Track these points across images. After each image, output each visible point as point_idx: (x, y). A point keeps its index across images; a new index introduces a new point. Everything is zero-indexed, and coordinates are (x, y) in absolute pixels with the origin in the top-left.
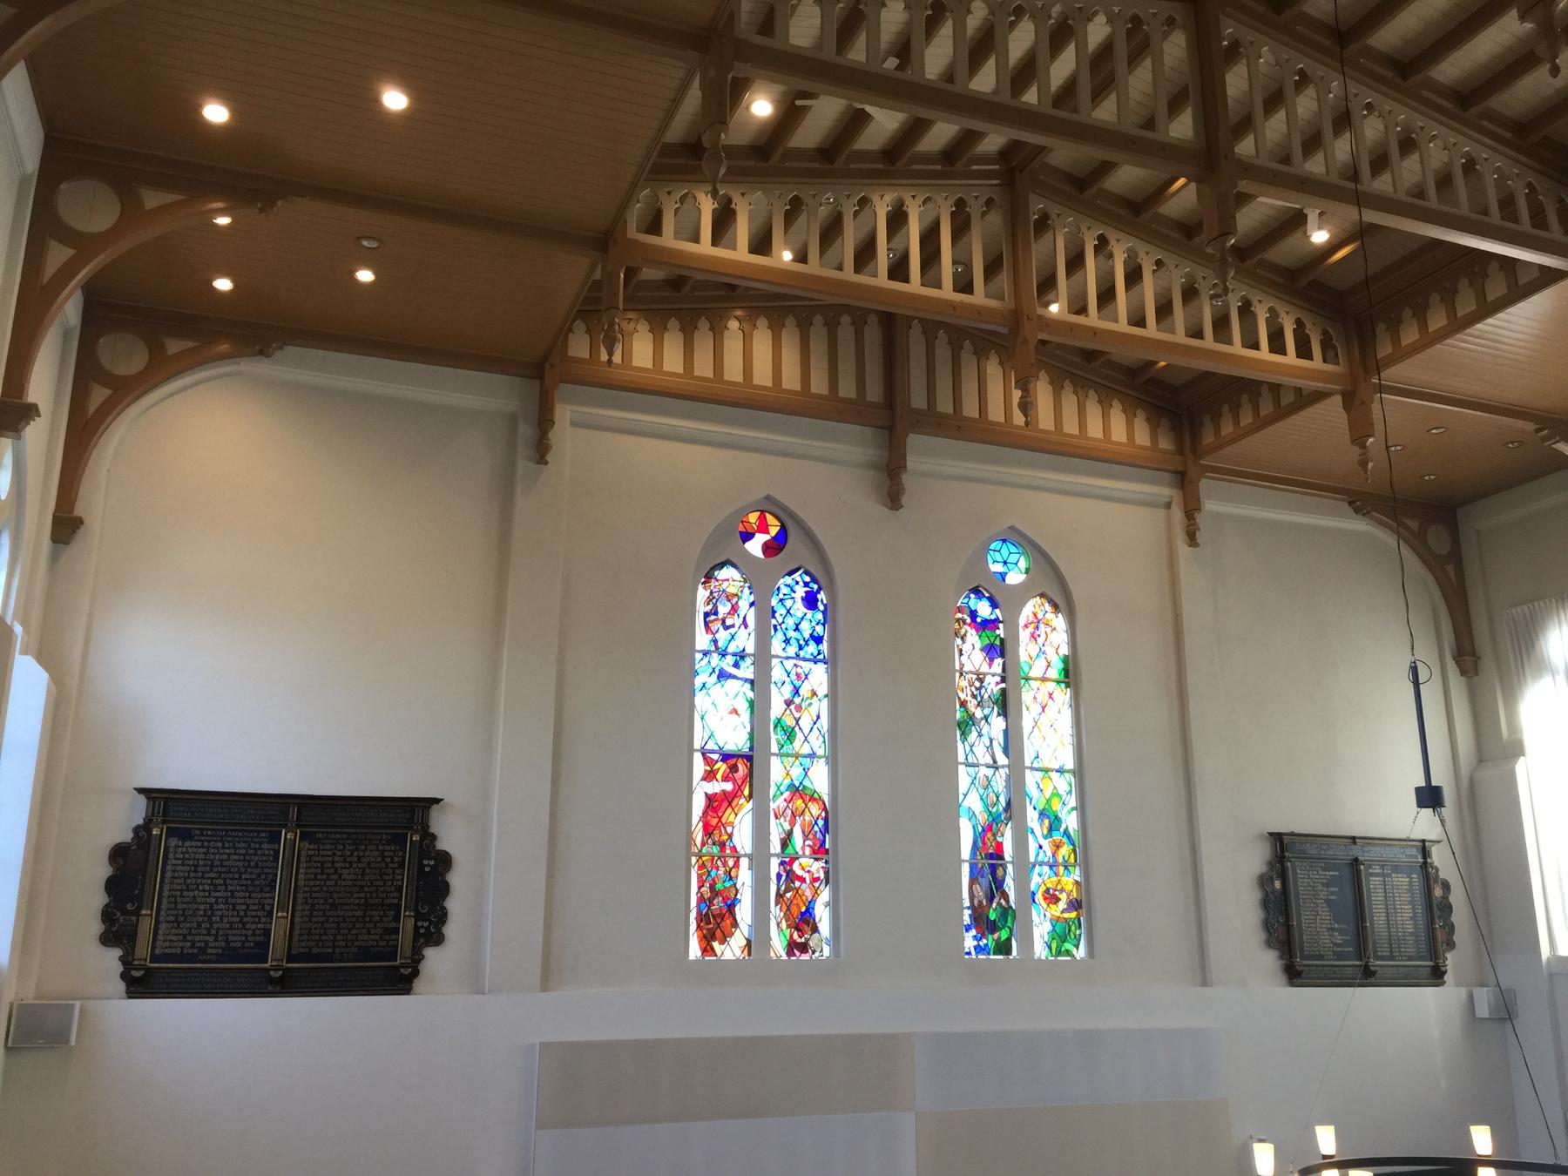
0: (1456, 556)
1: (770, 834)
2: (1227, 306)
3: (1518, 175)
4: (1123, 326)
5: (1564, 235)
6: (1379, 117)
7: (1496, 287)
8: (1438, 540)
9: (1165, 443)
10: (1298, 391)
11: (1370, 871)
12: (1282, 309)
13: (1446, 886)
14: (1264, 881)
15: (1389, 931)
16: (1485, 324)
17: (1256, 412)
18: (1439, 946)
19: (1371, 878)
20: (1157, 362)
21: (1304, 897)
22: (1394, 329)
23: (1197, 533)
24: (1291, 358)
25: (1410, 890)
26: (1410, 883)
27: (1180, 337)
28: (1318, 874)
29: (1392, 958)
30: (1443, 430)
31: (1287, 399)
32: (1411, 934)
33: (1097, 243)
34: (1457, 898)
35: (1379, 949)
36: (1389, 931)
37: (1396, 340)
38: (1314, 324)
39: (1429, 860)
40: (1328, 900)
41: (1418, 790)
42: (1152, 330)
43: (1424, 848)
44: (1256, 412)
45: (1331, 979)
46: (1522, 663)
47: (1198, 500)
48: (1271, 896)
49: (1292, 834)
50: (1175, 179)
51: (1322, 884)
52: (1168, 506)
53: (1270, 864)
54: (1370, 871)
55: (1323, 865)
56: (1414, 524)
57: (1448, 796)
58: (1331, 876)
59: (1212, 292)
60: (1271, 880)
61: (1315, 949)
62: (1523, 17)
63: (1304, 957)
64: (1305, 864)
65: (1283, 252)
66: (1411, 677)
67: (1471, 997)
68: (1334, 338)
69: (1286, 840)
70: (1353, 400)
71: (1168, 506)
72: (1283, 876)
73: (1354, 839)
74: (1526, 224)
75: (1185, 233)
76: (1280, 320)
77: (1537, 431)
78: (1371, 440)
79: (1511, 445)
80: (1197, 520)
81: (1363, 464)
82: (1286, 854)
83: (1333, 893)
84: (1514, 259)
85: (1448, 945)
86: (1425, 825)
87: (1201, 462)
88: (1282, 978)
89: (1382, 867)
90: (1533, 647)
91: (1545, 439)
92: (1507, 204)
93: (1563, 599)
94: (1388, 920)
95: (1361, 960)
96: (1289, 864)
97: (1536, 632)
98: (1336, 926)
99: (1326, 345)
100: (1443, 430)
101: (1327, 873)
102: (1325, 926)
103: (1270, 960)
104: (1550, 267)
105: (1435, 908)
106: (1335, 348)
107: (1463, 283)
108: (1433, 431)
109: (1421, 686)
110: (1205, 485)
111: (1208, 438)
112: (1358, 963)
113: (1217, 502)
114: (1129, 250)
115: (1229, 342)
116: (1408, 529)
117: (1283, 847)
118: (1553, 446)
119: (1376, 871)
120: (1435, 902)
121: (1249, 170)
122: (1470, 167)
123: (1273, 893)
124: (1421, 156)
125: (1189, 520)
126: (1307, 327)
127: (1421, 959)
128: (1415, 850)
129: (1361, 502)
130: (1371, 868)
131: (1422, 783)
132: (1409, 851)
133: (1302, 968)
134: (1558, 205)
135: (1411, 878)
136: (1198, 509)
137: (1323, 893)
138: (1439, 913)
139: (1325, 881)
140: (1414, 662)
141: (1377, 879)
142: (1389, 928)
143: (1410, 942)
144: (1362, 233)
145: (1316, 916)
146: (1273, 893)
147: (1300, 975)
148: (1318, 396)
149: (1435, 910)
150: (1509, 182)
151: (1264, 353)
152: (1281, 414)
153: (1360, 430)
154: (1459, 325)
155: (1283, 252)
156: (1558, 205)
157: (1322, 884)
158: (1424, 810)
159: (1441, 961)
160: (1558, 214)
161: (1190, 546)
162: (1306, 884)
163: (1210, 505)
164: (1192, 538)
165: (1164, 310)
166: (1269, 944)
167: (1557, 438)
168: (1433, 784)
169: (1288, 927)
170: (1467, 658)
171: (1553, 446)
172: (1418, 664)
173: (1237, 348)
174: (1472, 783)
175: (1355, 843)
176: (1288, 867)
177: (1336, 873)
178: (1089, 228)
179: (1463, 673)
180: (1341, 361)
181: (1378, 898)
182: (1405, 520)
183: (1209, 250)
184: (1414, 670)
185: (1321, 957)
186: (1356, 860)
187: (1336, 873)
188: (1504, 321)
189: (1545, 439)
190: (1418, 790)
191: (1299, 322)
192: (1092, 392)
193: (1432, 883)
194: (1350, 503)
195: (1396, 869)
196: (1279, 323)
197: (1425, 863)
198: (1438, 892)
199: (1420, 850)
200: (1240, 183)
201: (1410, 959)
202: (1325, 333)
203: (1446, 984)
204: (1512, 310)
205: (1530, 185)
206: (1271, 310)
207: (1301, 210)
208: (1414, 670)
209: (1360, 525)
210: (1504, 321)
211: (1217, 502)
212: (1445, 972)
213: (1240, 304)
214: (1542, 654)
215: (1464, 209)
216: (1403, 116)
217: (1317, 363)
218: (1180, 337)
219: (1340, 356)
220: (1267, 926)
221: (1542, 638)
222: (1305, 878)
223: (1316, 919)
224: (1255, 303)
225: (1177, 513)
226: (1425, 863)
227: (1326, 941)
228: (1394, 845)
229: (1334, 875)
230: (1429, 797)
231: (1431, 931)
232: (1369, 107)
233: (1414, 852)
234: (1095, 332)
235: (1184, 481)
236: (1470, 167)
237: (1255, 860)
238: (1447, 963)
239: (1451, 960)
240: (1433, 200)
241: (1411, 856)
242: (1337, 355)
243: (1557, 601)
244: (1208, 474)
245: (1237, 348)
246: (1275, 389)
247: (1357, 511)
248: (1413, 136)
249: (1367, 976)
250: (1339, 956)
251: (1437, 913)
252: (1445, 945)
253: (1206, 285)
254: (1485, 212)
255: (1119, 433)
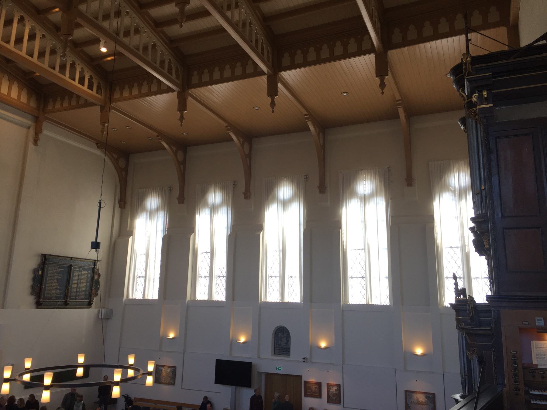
0: (126, 169)
1: (295, 303)
2: (66, 60)
3: (167, 55)
4: (23, 53)
5: (176, 79)
6: (130, 17)
7: (154, 88)
8: (122, 163)
9: (33, 104)
10: (86, 100)
11: (75, 269)
12: (86, 69)
13: (99, 275)
14: (35, 271)
15: (77, 290)
16: (149, 98)
17: (70, 103)
18: (92, 295)
19: (75, 272)
20: (35, 73)
21: (49, 277)
22: (122, 90)
23: (38, 141)
24: (85, 88)
25: (87, 277)
26: (88, 274)
27: (46, 66)
28: (56, 269)
29: (76, 299)
30: (130, 128)
31: (82, 102)
32: (84, 291)
33: (19, 18)
34: (102, 280)
35: (72, 296)
36: (77, 290)
37: (121, 94)
38: (96, 79)
39: (95, 267)
40: (58, 279)
41: (92, 243)
42: (35, 59)
43: (95, 262)
44: (70, 103)
45: (53, 306)
46: (138, 206)
47: (41, 129)
48: (37, 276)
49: (50, 255)
50: (56, 8)
51: (57, 273)
52: (29, 128)
53: (39, 265)
54: (75, 269)
55: (59, 266)
56: (115, 156)
57: (102, 246)
58: (61, 270)
59: (62, 54)
60: (38, 271)
61: (49, 296)
62: (176, 5)
63: (44, 298)
64: (52, 266)
65: (90, 50)
66: (98, 205)
67: (99, 311)
68: (102, 86)
69: (47, 257)
70: (105, 109)
71: (29, 128)
72: (43, 270)
73: (72, 258)
74: (166, 71)
75: (55, 29)
76: (84, 73)
77: (226, 127)
78: (186, 111)
79: (149, 138)
80: (39, 136)
81: (102, 132)
82: (46, 262)
83: (60, 276)
84: (161, 81)
85: (95, 294)
86: (93, 255)
87: (45, 115)
88: (35, 306)
89: (79, 268)
90: (142, 202)
91: (159, 139)
92: (162, 62)
93: (154, 189)
94: (77, 286)
95: (65, 300)
96: (72, 268)
97: (144, 198)
98: (58, 288)
99: (99, 88)
100: (130, 128)
101: (59, 269)
102: (54, 288)
103: (31, 299)
104: (170, 87)
105: (94, 283)
106: (101, 89)
107: (145, 83)
108: (127, 127)
109: (101, 208)
110: (45, 124)
111: (50, 107)
112: (64, 300)
113: (48, 131)
114: (32, 26)
115: (64, 74)
116: (113, 157)
117: (45, 259)
118: (161, 142)
119: (77, 269)
120: (94, 281)
121: (81, 15)
122: (154, 46)
123: (38, 275)
124: (140, 36)
125: (36, 135)
126: (93, 79)
127: (85, 299)
128: (92, 263)
129: (102, 145)
130: (75, 268)
131: (94, 241)
132: (89, 263)
133: (42, 302)
134: (176, 69)
135: (88, 272)
136: (41, 132)
137: (56, 276)
138: (95, 284)
139: (58, 272)
140: (101, 200)
141: (77, 272)
142: (77, 289)
143: (83, 294)
144: (115, 54)
145: (52, 284)
146: (38, 275)
147: (41, 305)
148: (93, 104)
149: (94, 283)
150: (164, 56)
151: (76, 83)
152: (79, 106)
153: (104, 119)
154: (347, 55)
155: (90, 50)
156: (176, 69)
157: (57, 273)
158: (93, 249)
159: (92, 300)
160: (97, 87)
161: (34, 145)
162: (51, 273)
163: (45, 132)
164: (36, 142)
165: (41, 54)
166: (32, 294)
167: (162, 140)
168: (98, 241)
169: (41, 288)
170: (123, 203)
171: (161, 142)
172: (102, 201)
173: (67, 78)
174: (115, 242)
175: (72, 259)
176: (45, 266)
177: (62, 270)
178: (17, 11)
179: (120, 207)
180: (102, 95)
181: (76, 279)
182: (113, 155)
183: (62, 38)
184: (100, 203)
185: (50, 299)
186: (71, 265)
187: (62, 270)
188: (151, 99)
189: (159, 139)
190: (92, 243)
191: (91, 76)
192: (6, 76)
193: (95, 274)
194: (96, 144)
195: (84, 269)
196: (84, 75)
197: (94, 268)
198: (96, 277)
199: (93, 263)
200: (78, 18)
201: (82, 299)
202: (99, 83)
203: (92, 308)
204: (356, 59)
205: (170, 60)
206: (82, 68)
207: (99, 38)
208: (100, 203)
209: (98, 152)
210: (151, 99)
211: (48, 131)
212: (92, 304)
213: (71, 62)
214: (145, 204)
215: (149, 58)
216: (137, 21)
217: (94, 93)
218: (46, 66)
219: (102, 93)
220: (33, 287)
221: (145, 200)
222: (51, 271)
223: (52, 285)
224: (77, 64)
225: (32, 132)
226: (94, 268)
227: (54, 293)
228: (85, 261)
229: (61, 270)
230: (96, 245)
231: (91, 290)
232: (127, 12)
233: (91, 264)
234: (11, 52)
235: (37, 120)
236: (154, 46)
237: (33, 263)
238: (94, 300)
239: (95, 300)
240: (141, 52)
241: (90, 265)
242: (101, 92)
243: (152, 189)
244: (47, 120)
245: (67, 78)
246: (78, 97)
247: (98, 147)
248: (139, 29)
249: (65, 305)
250: (58, 298)
251: (94, 284)
252: (94, 295)
253: (60, 52)
254: (155, 63)
255: (14, 94)
